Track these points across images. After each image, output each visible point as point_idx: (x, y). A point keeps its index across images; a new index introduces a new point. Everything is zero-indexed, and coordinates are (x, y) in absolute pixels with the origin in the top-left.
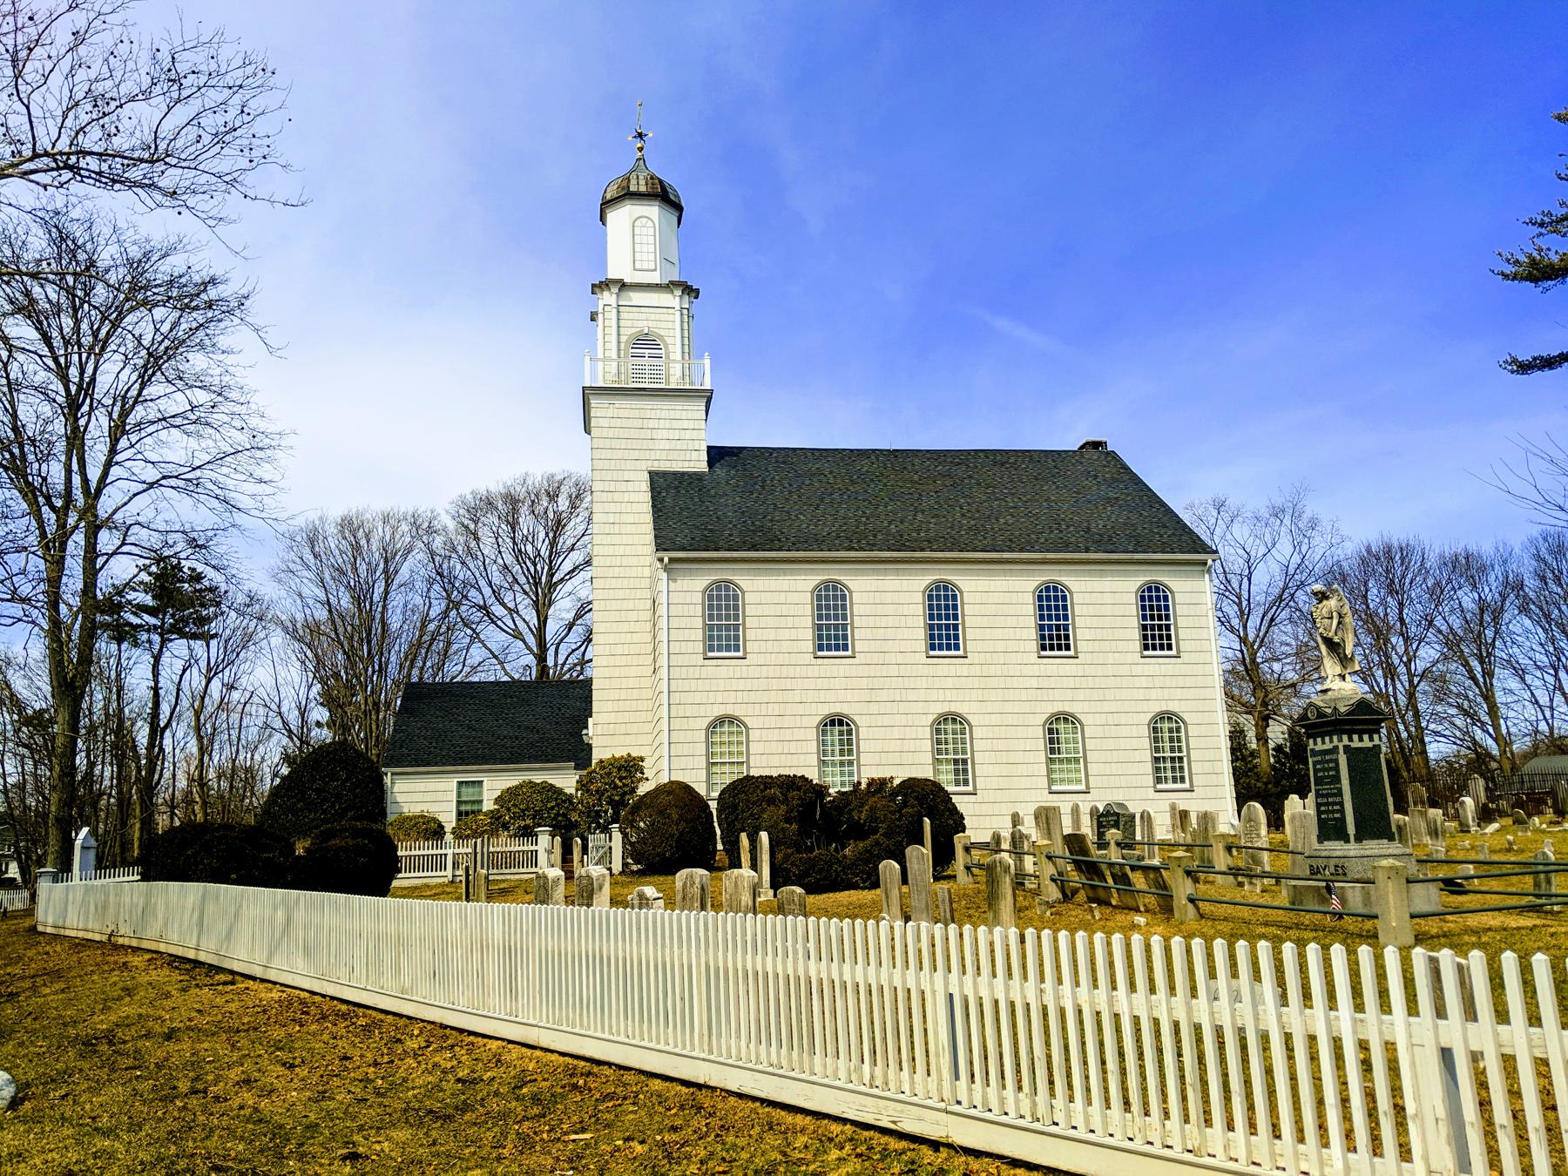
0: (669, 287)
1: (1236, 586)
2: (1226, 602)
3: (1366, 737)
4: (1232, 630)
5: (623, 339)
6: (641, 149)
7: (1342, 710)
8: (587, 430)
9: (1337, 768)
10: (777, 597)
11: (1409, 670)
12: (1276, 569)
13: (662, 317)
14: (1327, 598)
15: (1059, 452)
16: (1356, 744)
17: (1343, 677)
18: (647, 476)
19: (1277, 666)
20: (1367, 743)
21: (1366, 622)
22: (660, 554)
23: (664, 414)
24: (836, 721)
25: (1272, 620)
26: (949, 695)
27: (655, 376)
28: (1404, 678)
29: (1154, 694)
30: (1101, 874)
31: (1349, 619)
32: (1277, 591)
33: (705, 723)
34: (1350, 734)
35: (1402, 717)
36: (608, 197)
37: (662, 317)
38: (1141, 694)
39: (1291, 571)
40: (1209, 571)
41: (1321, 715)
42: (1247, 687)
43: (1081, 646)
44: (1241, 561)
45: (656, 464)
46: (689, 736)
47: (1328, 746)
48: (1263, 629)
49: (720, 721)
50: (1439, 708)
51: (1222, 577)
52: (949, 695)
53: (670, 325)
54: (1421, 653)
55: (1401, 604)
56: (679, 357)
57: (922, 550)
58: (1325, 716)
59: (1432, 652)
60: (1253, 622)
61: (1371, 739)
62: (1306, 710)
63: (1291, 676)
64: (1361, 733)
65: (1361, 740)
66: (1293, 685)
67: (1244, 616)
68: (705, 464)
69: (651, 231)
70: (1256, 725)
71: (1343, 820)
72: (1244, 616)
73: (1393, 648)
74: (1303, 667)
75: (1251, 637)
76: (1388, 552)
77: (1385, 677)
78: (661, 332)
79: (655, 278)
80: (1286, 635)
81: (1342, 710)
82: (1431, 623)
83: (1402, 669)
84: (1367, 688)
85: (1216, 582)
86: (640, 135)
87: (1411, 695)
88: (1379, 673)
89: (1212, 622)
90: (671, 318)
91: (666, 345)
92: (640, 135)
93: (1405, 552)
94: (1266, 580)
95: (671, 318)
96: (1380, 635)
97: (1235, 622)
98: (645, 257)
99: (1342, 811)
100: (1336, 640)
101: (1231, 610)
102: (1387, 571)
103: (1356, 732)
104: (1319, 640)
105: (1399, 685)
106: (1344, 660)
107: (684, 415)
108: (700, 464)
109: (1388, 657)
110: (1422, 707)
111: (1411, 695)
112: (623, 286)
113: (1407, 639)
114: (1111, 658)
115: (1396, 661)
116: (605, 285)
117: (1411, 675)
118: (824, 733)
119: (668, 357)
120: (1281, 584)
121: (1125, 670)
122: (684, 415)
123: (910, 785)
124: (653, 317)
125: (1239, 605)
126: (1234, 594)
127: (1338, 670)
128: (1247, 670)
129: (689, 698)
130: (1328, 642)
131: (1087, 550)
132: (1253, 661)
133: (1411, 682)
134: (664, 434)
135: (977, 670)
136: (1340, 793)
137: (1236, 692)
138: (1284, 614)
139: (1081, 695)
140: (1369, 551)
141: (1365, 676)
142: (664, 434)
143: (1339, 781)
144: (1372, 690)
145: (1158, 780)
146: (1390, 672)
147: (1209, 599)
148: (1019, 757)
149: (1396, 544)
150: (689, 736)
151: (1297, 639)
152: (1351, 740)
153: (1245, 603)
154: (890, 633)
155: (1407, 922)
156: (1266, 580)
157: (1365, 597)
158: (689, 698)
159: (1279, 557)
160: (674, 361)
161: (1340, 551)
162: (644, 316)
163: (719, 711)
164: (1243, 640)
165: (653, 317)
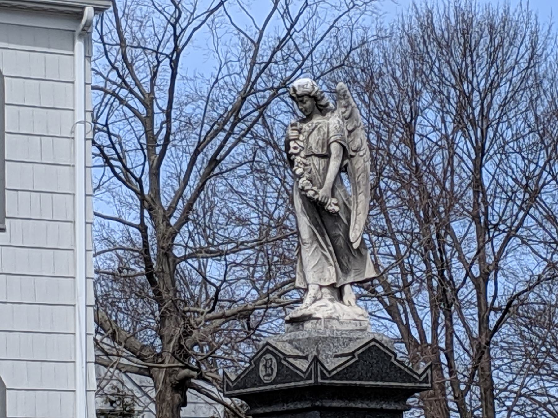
1: (144, 76)
2: (120, 111)
4: (127, 177)
7: (331, 364)
11: (481, 293)
12: (234, 48)
14: (323, 110)
17: (338, 292)
19: (214, 269)
21: (406, 185)
25: (214, 162)
28: (471, 313)
31: (362, 162)
32: (229, 98)
35: (459, 399)
39: (264, 53)
40: (85, 34)
41: (286, 371)
42: (151, 312)
44: (159, 20)
48: (194, 182)
50: (533, 384)
51: (114, 52)
54: (510, 262)
55: (481, 151)
58: (294, 375)
59: (530, 260)
60: (173, 164)
62: (255, 361)
63: (245, 293)
66: (245, 314)
67: (155, 148)
70: (159, 401)
72: (155, 148)
73: (456, 245)
74: (268, 277)
75: (166, 198)
76: (465, 28)
77: (434, 307)
80: (240, 198)
81: (331, 364)
82: (534, 196)
83: (468, 292)
84: (395, 331)
85: (102, 64)
87: (481, 351)
88: (422, 299)
89: (81, 152)
93: (501, 33)
94: (209, 70)
96: (433, 214)
97: (136, 160)
100: (332, 206)
101: (129, 132)
102: (461, 77)
104: (298, 202)
105: (459, 328)
106: (345, 255)
109: (444, 265)
110: (500, 378)
111: (481, 351)
113: (485, 230)
115: (459, 275)
117: (484, 309)
120: (241, 83)
125: (148, 121)
126: (136, 90)
127: (330, 274)
128: (150, 276)
130: (316, 208)
132: (166, 253)
133: (483, 321)
137: (125, 324)
138: (241, 151)
140: (428, 26)
141: (396, 307)
144: (405, 329)
146: (445, 300)
147: (80, 100)
149: (480, 15)
151: (263, 212)
153: (159, 118)
156: (208, 68)
157: (410, 128)
159: (242, 22)
161: (367, 20)
164: (148, 203)
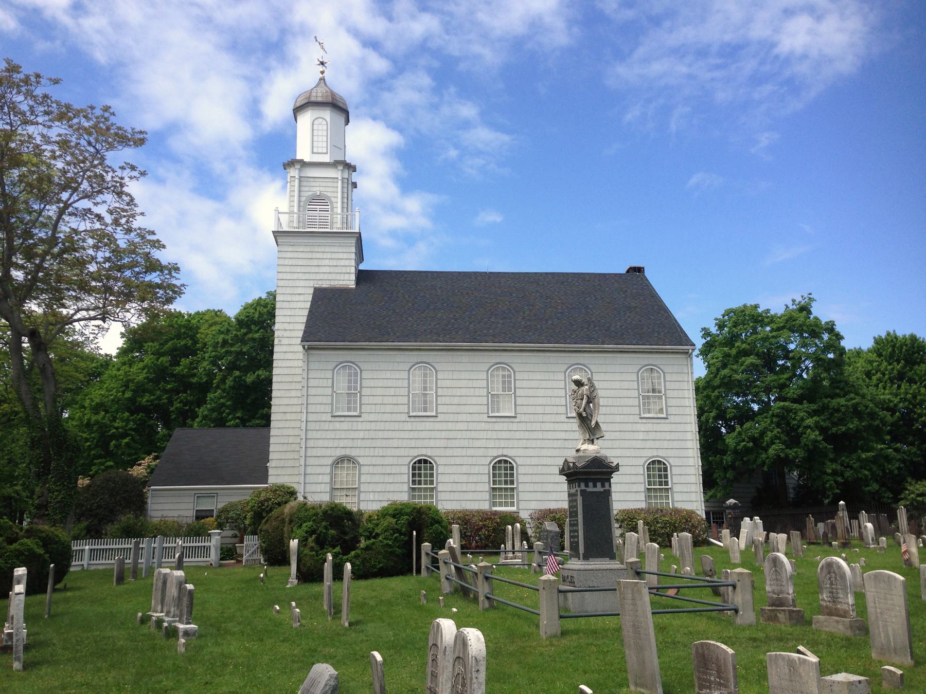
0: (335, 164)
3: (599, 484)
5: (303, 199)
6: (322, 73)
13: (329, 184)
15: (604, 275)
16: (591, 489)
20: (599, 488)
26: (503, 444)
27: (324, 224)
29: (649, 444)
33: (330, 461)
36: (298, 105)
37: (329, 184)
38: (639, 444)
46: (319, 470)
49: (340, 461)
52: (503, 444)
53: (335, 190)
56: (339, 211)
61: (603, 486)
65: (595, 486)
69: (325, 127)
78: (329, 194)
79: (326, 159)
86: (322, 63)
90: (335, 185)
91: (332, 203)
92: (322, 63)
95: (335, 185)
98: (320, 144)
103: (591, 480)
108: (349, 281)
112: (303, 164)
114: (618, 419)
116: (292, 163)
119: (332, 210)
123: (396, 511)
129: (321, 443)
134: (326, 262)
135: (523, 427)
142: (326, 262)
143: (577, 516)
150: (319, 470)
152: (587, 486)
154: (463, 400)
155: (557, 621)
158: (321, 443)
160: (337, 214)
162: (317, 184)
163: (339, 453)
165: (323, 184)
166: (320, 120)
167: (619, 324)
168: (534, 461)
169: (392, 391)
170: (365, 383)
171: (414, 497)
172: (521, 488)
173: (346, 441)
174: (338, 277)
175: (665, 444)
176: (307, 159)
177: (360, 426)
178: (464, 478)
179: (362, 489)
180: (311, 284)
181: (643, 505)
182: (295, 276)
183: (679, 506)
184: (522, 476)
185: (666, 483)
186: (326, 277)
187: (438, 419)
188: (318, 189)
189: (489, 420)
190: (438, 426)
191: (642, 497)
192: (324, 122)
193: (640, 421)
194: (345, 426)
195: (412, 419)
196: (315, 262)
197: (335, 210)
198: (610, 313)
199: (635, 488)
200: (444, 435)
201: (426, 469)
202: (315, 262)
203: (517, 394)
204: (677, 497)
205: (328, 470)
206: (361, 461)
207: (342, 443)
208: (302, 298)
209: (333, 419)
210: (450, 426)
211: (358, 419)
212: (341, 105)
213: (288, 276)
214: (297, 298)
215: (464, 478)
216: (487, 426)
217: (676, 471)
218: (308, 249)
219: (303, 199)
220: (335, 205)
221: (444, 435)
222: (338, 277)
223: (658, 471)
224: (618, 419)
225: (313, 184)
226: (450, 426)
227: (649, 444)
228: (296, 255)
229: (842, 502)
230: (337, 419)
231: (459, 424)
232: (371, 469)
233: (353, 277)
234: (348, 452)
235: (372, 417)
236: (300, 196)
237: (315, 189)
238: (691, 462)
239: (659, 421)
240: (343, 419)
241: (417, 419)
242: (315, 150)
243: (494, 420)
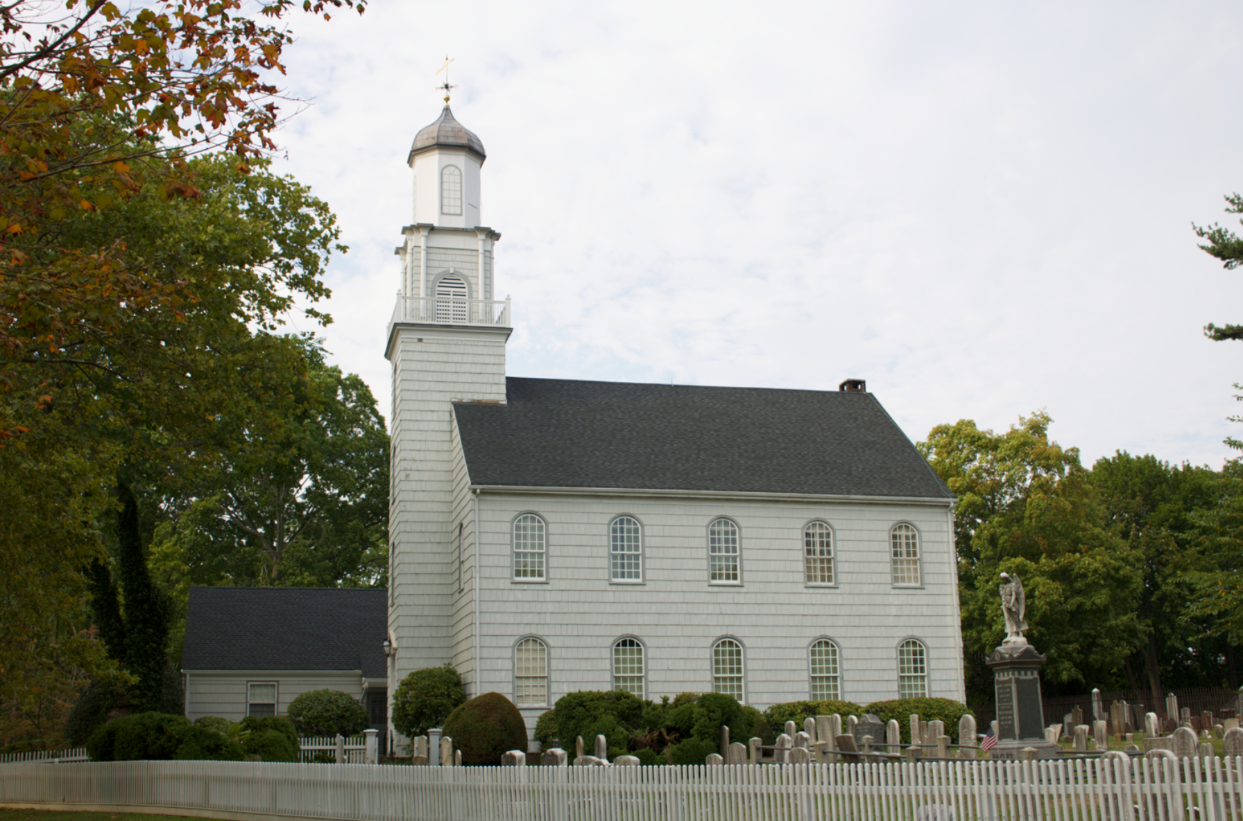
8: (388, 354)
9: (1010, 693)
10: (578, 527)
13: (467, 259)
16: (1023, 677)
18: (450, 407)
22: (475, 486)
23: (468, 349)
24: (628, 642)
26: (728, 620)
29: (902, 621)
30: (878, 734)
33: (511, 641)
34: (1019, 670)
36: (419, 145)
37: (467, 259)
38: (891, 621)
43: (842, 578)
45: (459, 396)
46: (497, 653)
47: (1006, 678)
52: (728, 620)
53: (474, 266)
57: (707, 489)
64: (1026, 670)
68: (504, 397)
71: (1012, 725)
78: (466, 273)
86: (447, 87)
90: (474, 259)
91: (470, 285)
99: (1012, 720)
106: (1018, 623)
107: (486, 351)
108: (499, 395)
114: (866, 589)
118: (617, 652)
119: (471, 296)
121: (879, 599)
122: (486, 351)
123: (705, 700)
124: (458, 258)
131: (849, 493)
134: (467, 368)
136: (1011, 709)
139: (840, 621)
142: (467, 368)
145: (809, 578)
148: (785, 676)
150: (497, 653)
162: (450, 258)
165: (458, 258)
166: (452, 169)
167: (861, 466)
168: (766, 643)
169: (588, 551)
170: (553, 540)
171: (718, 687)
172: (750, 676)
173: (530, 616)
174: (483, 388)
175: (922, 621)
176: (436, 224)
177: (548, 596)
178: (681, 665)
179: (553, 678)
180: (448, 397)
181: (896, 697)
182: (426, 386)
183: (934, 696)
184: (753, 662)
185: (922, 670)
186: (467, 388)
187: (646, 588)
188: (451, 264)
189: (710, 589)
190: (646, 597)
191: (806, 687)
192: (457, 172)
193: (893, 591)
194: (529, 596)
195: (614, 588)
196: (452, 368)
197: (474, 295)
198: (817, 446)
199: (886, 676)
200: (654, 608)
201: (827, 653)
202: (452, 368)
203: (745, 557)
204: (848, 687)
205: (508, 653)
206: (550, 641)
207: (527, 618)
208: (435, 416)
209: (514, 587)
210: (662, 597)
211: (545, 587)
212: (477, 147)
213: (416, 386)
214: (429, 416)
215: (681, 665)
216: (709, 598)
217: (933, 654)
218: (442, 348)
219: (432, 278)
220: (474, 287)
221: (654, 608)
222: (483, 388)
223: (913, 654)
224: (866, 589)
225: (443, 257)
226: (662, 597)
227: (902, 621)
228: (425, 357)
229: (1095, 690)
230: (519, 587)
231: (673, 595)
232: (564, 653)
233: (503, 389)
234: (534, 630)
235: (563, 585)
236: (427, 274)
237: (446, 264)
238: (951, 642)
239: (827, 591)
240: (526, 587)
241: (620, 588)
242: (446, 210)
243: (716, 589)
